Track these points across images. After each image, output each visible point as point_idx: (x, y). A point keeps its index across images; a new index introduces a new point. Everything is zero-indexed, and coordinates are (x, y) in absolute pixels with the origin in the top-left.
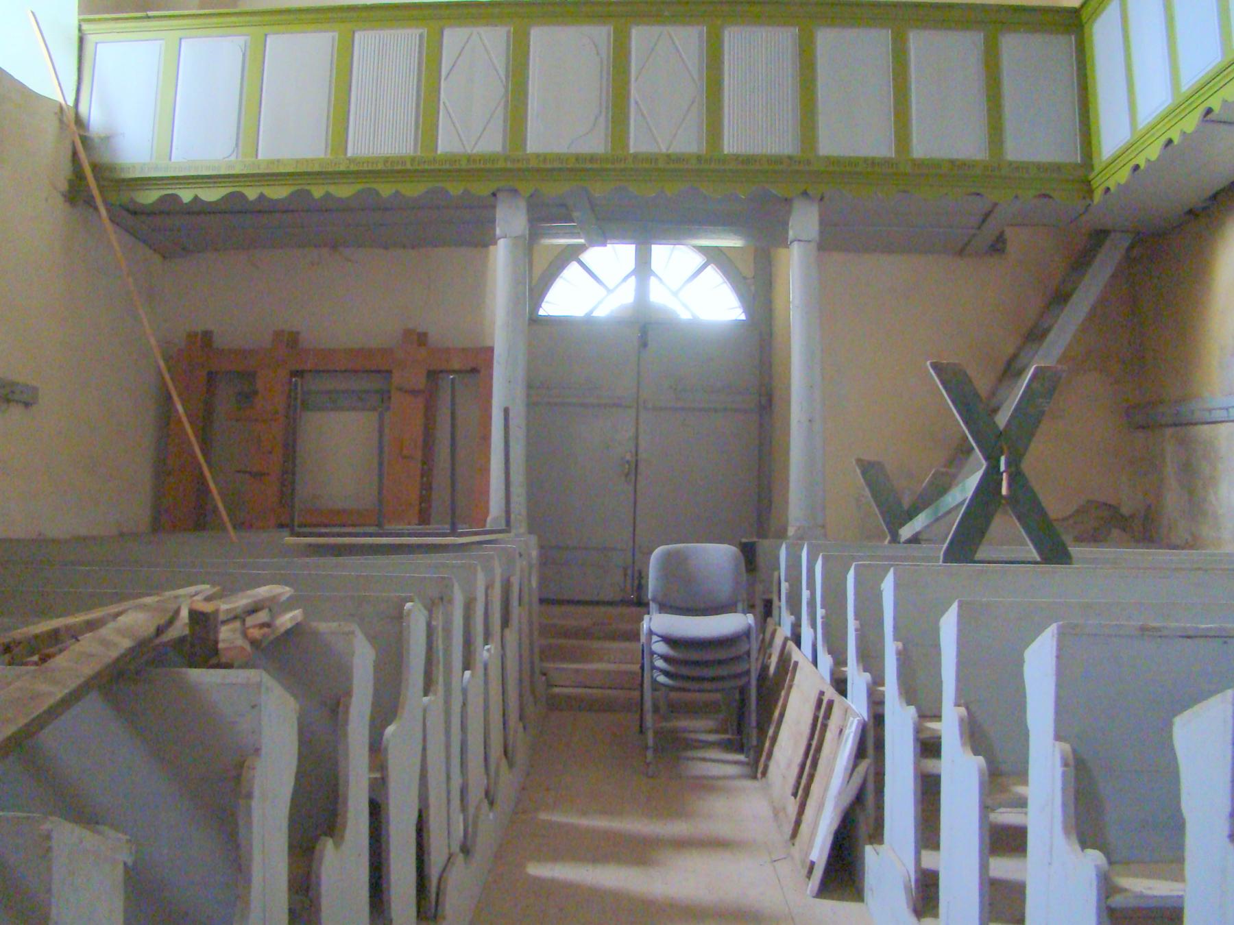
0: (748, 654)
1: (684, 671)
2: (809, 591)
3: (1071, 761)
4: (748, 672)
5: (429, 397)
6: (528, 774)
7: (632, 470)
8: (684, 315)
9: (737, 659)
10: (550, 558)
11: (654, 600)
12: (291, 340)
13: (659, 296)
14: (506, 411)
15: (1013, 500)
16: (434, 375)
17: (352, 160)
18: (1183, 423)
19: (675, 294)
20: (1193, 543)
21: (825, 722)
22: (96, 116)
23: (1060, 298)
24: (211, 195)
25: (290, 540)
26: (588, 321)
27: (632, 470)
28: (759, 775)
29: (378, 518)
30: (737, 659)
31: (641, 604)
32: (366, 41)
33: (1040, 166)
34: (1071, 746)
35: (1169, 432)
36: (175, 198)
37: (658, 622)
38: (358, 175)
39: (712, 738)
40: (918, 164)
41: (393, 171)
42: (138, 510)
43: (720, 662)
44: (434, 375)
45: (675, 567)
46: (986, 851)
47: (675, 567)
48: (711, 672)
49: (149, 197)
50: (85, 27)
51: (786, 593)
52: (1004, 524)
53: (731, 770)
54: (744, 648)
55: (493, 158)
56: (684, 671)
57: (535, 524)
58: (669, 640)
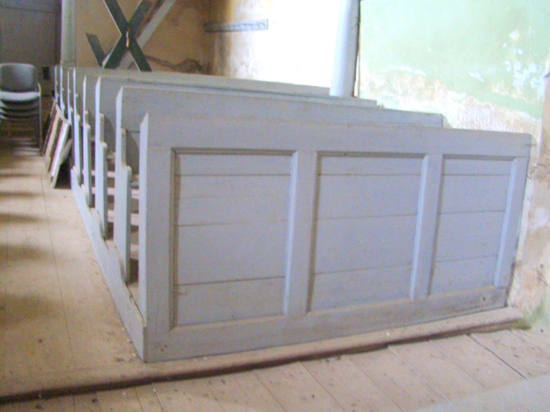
0: (38, 107)
1: (11, 114)
3: (103, 119)
4: (38, 115)
6: (236, 401)
9: (33, 109)
15: (131, 48)
18: (222, 31)
20: (222, 74)
21: (110, 157)
28: (43, 154)
30: (33, 109)
34: (104, 114)
35: (217, 34)
39: (28, 143)
43: (25, 111)
46: (107, 169)
48: (21, 114)
51: (70, 94)
52: (129, 58)
53: (33, 153)
54: (35, 105)
56: (11, 114)
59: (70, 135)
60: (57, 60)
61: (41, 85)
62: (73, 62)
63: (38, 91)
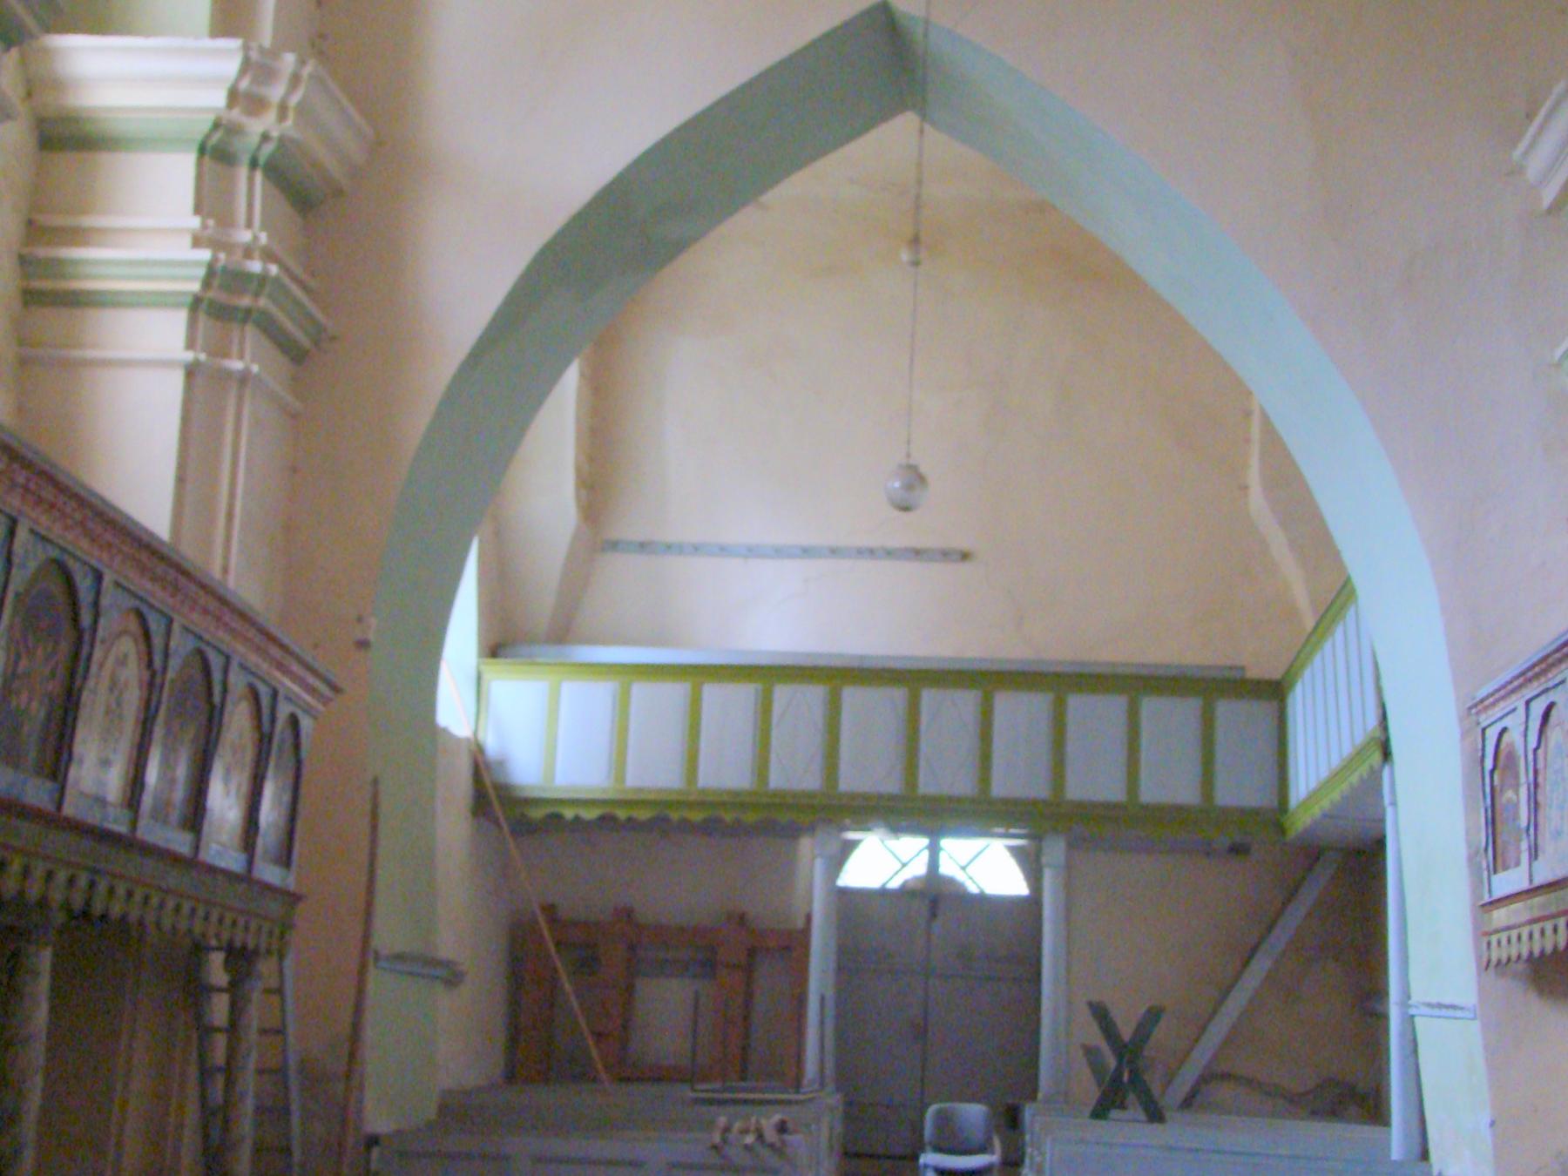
2: (839, 1096)
5: (749, 970)
7: (920, 1031)
8: (973, 889)
10: (853, 1111)
11: (930, 1143)
12: (627, 914)
13: (947, 868)
14: (823, 999)
16: (752, 952)
17: (704, 791)
19: (963, 868)
22: (491, 744)
23: (1292, 894)
24: (590, 814)
25: (692, 1095)
26: (883, 893)
27: (920, 1031)
31: (922, 1149)
32: (713, 693)
33: (1243, 812)
36: (559, 817)
37: (929, 1158)
40: (1145, 807)
41: (737, 801)
42: (495, 1066)
44: (752, 952)
45: (943, 1119)
47: (943, 1119)
49: (537, 814)
50: (483, 668)
55: (811, 795)
60: (1032, 1096)
61: (1002, 1142)
63: (993, 1153)
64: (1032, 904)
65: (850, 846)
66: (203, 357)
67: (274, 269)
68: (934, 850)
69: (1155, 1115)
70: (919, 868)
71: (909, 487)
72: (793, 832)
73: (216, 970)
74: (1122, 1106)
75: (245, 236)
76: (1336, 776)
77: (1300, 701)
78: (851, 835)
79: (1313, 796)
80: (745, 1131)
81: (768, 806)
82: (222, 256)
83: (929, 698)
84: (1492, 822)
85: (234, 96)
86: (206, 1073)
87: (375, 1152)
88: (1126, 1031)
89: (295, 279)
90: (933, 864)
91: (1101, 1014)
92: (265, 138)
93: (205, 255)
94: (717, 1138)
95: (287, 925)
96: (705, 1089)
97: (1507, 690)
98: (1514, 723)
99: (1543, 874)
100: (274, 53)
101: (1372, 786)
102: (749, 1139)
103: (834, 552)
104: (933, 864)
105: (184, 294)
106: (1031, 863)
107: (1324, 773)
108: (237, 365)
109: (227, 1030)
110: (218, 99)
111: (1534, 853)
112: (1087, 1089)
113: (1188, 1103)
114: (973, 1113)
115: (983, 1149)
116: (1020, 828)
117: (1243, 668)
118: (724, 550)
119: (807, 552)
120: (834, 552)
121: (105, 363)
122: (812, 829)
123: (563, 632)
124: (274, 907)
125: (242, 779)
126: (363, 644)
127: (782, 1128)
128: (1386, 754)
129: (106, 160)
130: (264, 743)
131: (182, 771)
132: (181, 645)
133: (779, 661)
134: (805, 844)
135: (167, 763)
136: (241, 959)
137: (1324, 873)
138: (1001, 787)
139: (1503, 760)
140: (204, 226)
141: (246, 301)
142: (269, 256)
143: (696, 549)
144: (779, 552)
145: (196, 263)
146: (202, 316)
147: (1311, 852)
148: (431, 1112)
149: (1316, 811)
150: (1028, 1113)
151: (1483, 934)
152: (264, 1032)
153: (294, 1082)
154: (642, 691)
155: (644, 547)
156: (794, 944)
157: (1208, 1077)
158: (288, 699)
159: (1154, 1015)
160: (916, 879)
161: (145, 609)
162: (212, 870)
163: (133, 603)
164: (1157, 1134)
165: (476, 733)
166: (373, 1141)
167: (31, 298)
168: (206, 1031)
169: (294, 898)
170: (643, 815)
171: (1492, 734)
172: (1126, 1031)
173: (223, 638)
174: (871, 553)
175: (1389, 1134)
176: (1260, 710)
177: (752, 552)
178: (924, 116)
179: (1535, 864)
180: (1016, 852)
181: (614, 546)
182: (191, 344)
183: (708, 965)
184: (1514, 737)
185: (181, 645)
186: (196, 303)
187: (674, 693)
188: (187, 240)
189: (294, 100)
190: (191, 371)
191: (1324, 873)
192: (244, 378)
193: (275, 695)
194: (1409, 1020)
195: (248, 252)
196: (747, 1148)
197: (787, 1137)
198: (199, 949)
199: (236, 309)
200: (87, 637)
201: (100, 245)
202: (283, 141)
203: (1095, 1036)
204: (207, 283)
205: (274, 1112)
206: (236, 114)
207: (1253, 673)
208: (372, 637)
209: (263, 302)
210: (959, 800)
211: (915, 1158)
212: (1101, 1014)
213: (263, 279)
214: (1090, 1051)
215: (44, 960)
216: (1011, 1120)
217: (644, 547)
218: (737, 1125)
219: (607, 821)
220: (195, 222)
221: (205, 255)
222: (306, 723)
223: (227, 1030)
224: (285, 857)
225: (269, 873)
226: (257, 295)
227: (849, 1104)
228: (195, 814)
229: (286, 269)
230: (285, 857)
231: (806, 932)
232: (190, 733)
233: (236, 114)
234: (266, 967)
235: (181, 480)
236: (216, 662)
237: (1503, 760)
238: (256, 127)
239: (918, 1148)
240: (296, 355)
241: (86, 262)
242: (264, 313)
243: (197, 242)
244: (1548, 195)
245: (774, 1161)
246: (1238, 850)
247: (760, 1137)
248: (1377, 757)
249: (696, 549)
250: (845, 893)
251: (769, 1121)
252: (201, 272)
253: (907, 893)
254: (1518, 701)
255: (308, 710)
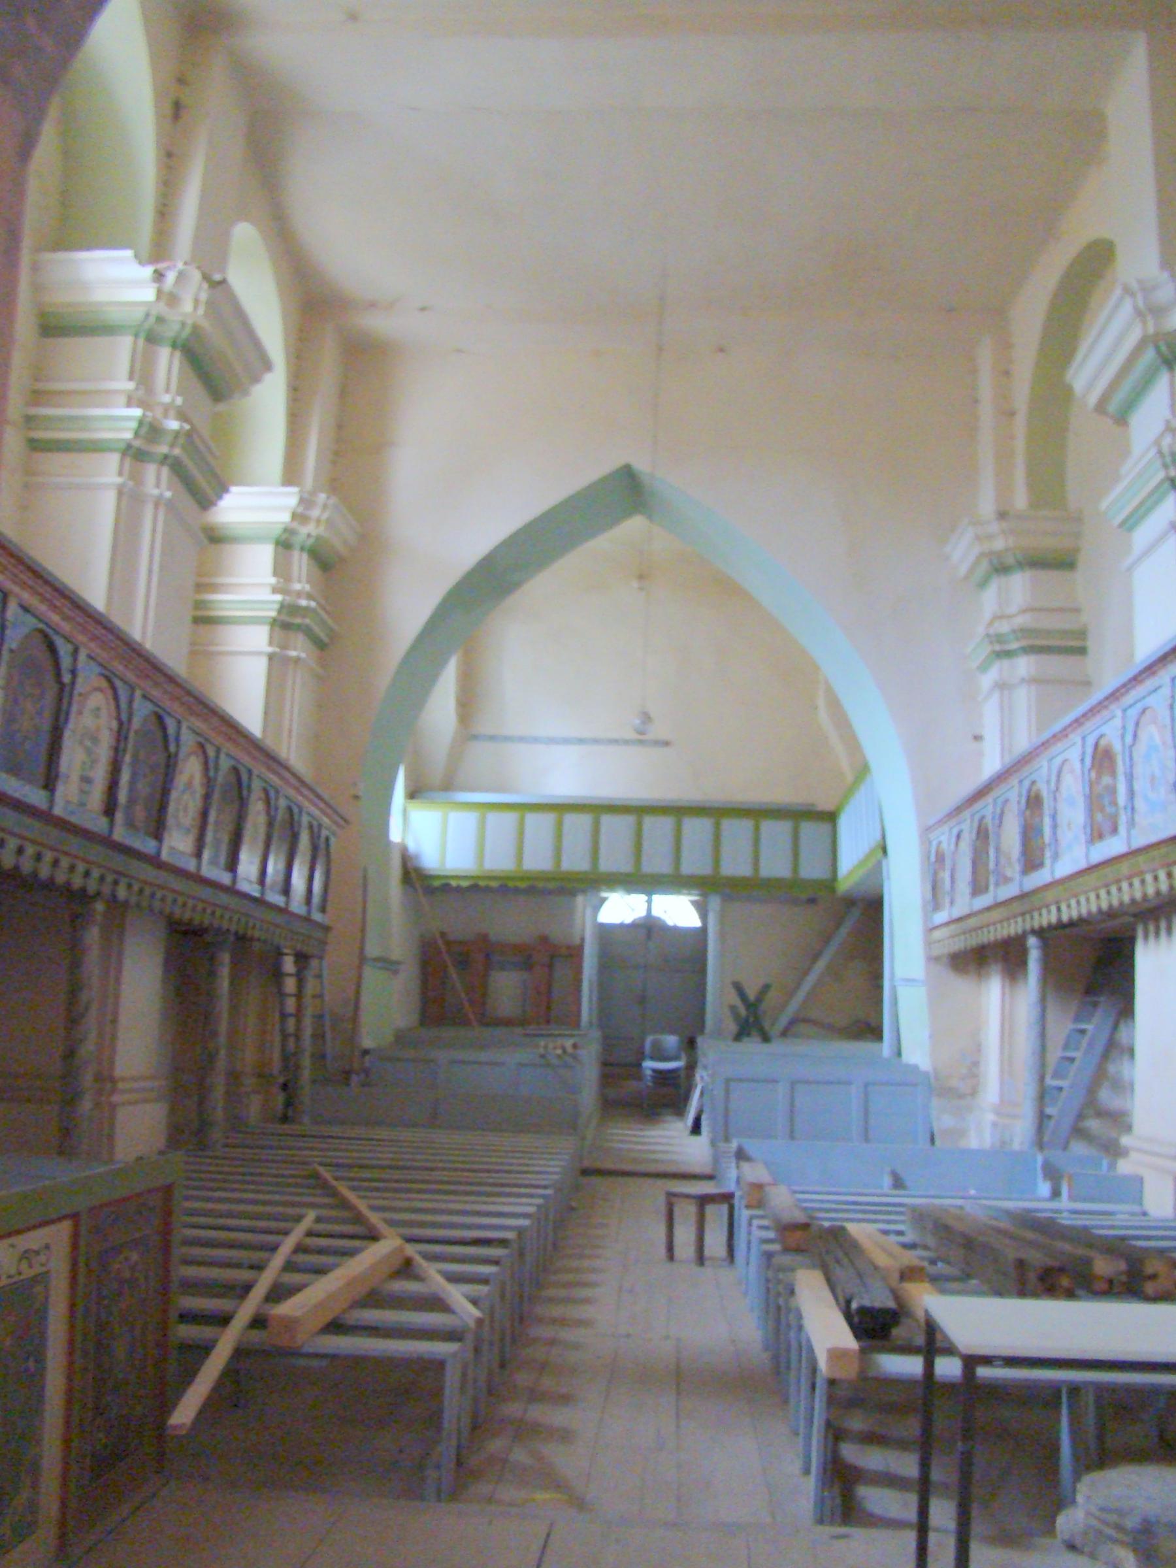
5: (550, 966)
7: (642, 999)
10: (608, 1044)
12: (485, 938)
13: (655, 912)
16: (552, 957)
17: (527, 871)
22: (412, 846)
24: (465, 884)
25: (524, 1032)
27: (642, 999)
29: (523, 1022)
32: (531, 819)
33: (815, 881)
36: (448, 885)
37: (649, 1064)
38: (528, 879)
42: (415, 1017)
44: (552, 957)
45: (656, 1045)
49: (437, 883)
57: (601, 1027)
58: (654, 1071)
59: (702, 1094)
60: (701, 1027)
62: (719, 1034)
64: (703, 930)
65: (604, 900)
66: (277, 650)
67: (313, 604)
68: (649, 902)
69: (766, 1038)
70: (641, 912)
71: (644, 723)
72: (573, 893)
73: (289, 965)
74: (749, 1035)
75: (297, 586)
76: (862, 863)
77: (845, 823)
78: (604, 894)
79: (850, 873)
80: (555, 1048)
81: (562, 879)
82: (288, 598)
83: (649, 821)
84: (934, 888)
85: (295, 516)
86: (284, 1016)
87: (367, 1058)
88: (752, 995)
89: (324, 609)
90: (649, 909)
91: (739, 988)
92: (309, 536)
93: (279, 597)
94: (542, 1051)
95: (324, 943)
96: (531, 1029)
97: (941, 822)
98: (944, 838)
99: (957, 912)
100: (313, 493)
101: (878, 866)
102: (559, 1052)
103: (596, 741)
104: (649, 909)
105: (268, 617)
106: (703, 912)
107: (856, 862)
108: (293, 653)
109: (295, 995)
110: (286, 517)
111: (952, 902)
112: (732, 1027)
113: (784, 1034)
114: (671, 1041)
115: (676, 1058)
116: (1135, 1246)
117: (813, 805)
118: (536, 740)
119: (581, 741)
120: (596, 741)
121: (220, 653)
122: (584, 891)
123: (448, 785)
124: (319, 934)
125: (306, 872)
126: (356, 797)
127: (575, 1046)
128: (884, 851)
129: (228, 548)
130: (315, 848)
131: (281, 866)
132: (282, 803)
133: (571, 801)
134: (580, 899)
135: (275, 864)
136: (302, 958)
137: (856, 913)
138: (687, 868)
139: (940, 858)
140: (278, 582)
141: (298, 621)
142: (310, 597)
143: (522, 739)
144: (566, 741)
145: (273, 602)
146: (277, 629)
147: (850, 902)
148: (392, 1039)
149: (855, 878)
150: (699, 1040)
151: (928, 944)
152: (314, 997)
153: (328, 1023)
154: (493, 817)
155: (492, 738)
156: (575, 953)
157: (793, 1022)
158: (327, 829)
159: (766, 988)
160: (640, 918)
161: (269, 788)
162: (292, 914)
163: (264, 785)
164: (765, 1048)
165: (403, 839)
166: (366, 1052)
167: (198, 621)
168: (282, 994)
169: (327, 929)
170: (494, 884)
171: (934, 843)
172: (752, 995)
173: (247, 760)
174: (615, 742)
175: (882, 1046)
176: (824, 828)
177: (552, 741)
178: (650, 518)
179: (1133, 832)
180: (694, 903)
181: (475, 737)
182: (271, 643)
183: (527, 965)
184: (944, 846)
185: (282, 803)
186: (274, 623)
187: (510, 818)
188: (269, 590)
189: (325, 516)
190: (271, 657)
191: (856, 913)
192: (297, 660)
193: (250, 772)
194: (894, 989)
195: (299, 594)
196: (559, 1056)
197: (579, 1052)
198: (280, 954)
199: (293, 624)
200: (67, 689)
201: (227, 593)
202: (318, 538)
203: (737, 1001)
204: (280, 611)
205: (319, 1036)
206: (295, 525)
207: (820, 808)
208: (360, 794)
209: (307, 621)
210: (663, 876)
211: (640, 1065)
212: (739, 988)
213: (307, 609)
214: (733, 1008)
215: (226, 957)
216: (690, 1044)
217: (492, 738)
218: (551, 1046)
219: (474, 888)
220: (273, 580)
221: (279, 597)
222: (333, 840)
223: (295, 995)
224: (323, 909)
225: (317, 916)
226: (172, 446)
227: (606, 1038)
228: (286, 890)
229: (318, 603)
230: (323, 909)
231: (581, 948)
232: (285, 848)
233: (295, 525)
234: (314, 963)
235: (266, 713)
236: (296, 810)
237: (940, 858)
238: (304, 530)
239: (641, 1056)
240: (321, 645)
241: (221, 601)
242: (307, 626)
243: (275, 590)
244: (963, 570)
245: (570, 1060)
246: (812, 901)
247: (564, 1051)
248: (880, 854)
249: (522, 739)
250: (602, 925)
251: (568, 1043)
252: (277, 606)
253: (634, 926)
254: (946, 828)
255: (334, 834)
